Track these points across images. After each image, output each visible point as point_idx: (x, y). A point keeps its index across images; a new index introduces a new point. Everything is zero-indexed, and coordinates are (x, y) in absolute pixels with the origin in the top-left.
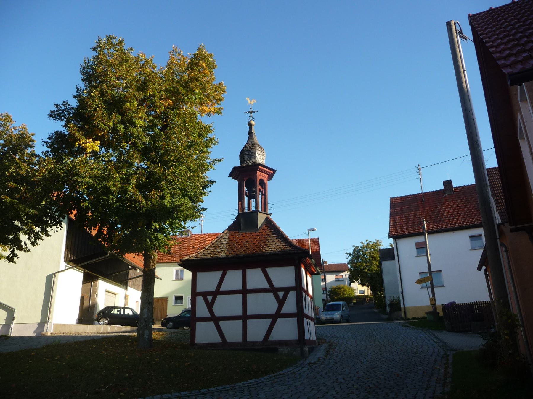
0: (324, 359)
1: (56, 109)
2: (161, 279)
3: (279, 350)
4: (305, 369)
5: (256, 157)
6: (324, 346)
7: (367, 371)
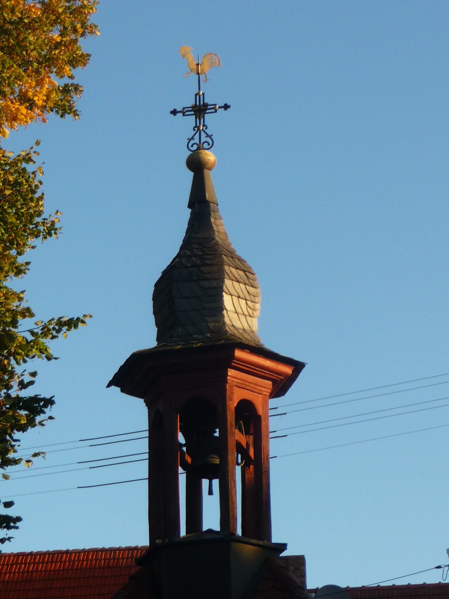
5: (220, 308)
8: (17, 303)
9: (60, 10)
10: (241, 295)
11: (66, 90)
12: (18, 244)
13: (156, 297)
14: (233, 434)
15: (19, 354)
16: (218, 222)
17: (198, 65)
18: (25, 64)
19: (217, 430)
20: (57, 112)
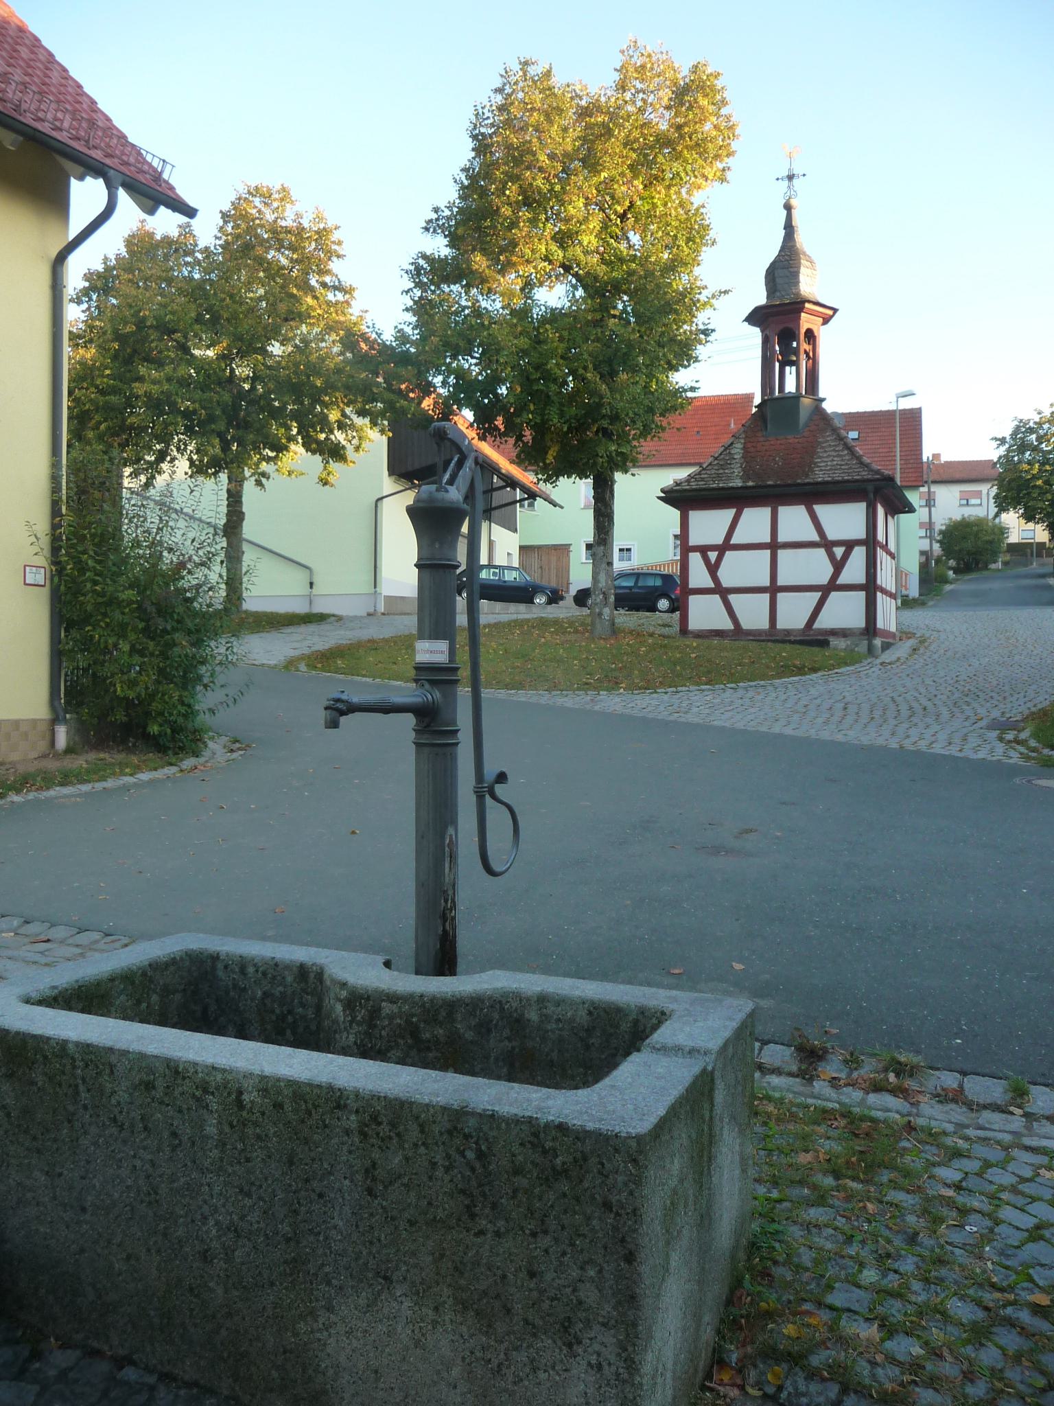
1: (434, 216)
2: (562, 507)
4: (873, 669)
6: (911, 643)
13: (766, 277)
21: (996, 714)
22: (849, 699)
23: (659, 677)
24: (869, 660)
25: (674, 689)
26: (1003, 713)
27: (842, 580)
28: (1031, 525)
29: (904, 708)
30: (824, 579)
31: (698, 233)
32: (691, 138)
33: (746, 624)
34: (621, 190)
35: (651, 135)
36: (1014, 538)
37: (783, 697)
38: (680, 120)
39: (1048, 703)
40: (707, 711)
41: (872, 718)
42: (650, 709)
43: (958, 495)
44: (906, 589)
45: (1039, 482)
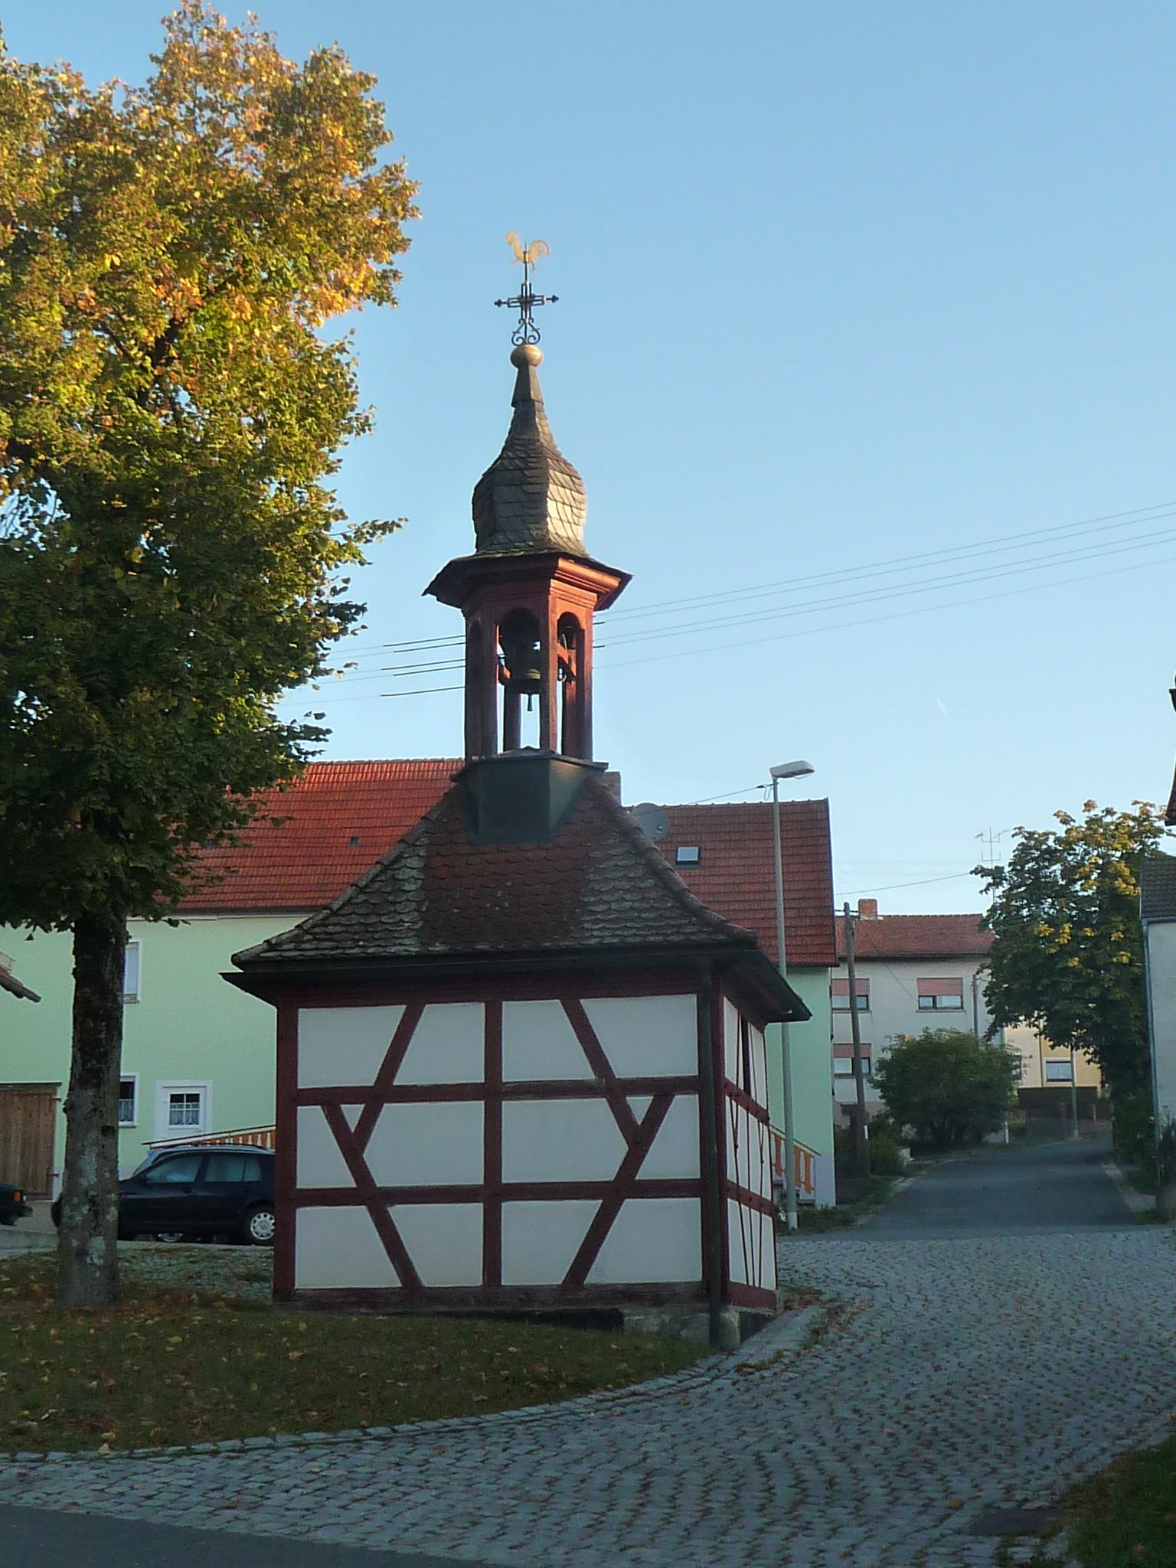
0: (798, 1355)
2: (35, 999)
3: (626, 1319)
4: (719, 1383)
5: (544, 515)
6: (810, 1314)
7: (947, 1393)
8: (330, 504)
9: (380, 191)
10: (567, 502)
11: (384, 276)
12: (330, 440)
14: (555, 648)
15: (331, 559)
16: (543, 423)
17: (525, 253)
18: (342, 251)
19: (538, 643)
20: (374, 300)
21: (992, 1491)
22: (655, 1461)
23: (203, 1411)
24: (713, 1360)
25: (236, 1443)
26: (1009, 1489)
27: (650, 1169)
28: (1063, 1052)
29: (782, 1483)
30: (606, 1169)
31: (326, 400)
32: (306, 200)
33: (430, 1276)
34: (147, 292)
35: (219, 189)
36: (1031, 1078)
37: (502, 1458)
38: (286, 166)
39: (1106, 1459)
40: (308, 1502)
41: (707, 1511)
42: (164, 1497)
43: (913, 987)
44: (809, 1189)
45: (1074, 962)
